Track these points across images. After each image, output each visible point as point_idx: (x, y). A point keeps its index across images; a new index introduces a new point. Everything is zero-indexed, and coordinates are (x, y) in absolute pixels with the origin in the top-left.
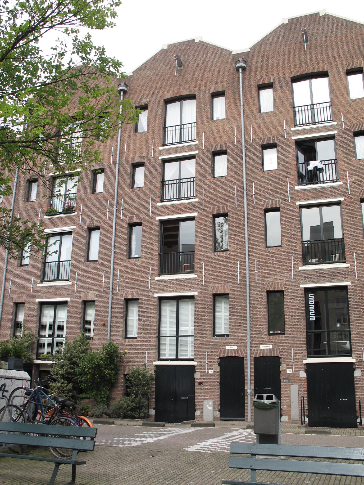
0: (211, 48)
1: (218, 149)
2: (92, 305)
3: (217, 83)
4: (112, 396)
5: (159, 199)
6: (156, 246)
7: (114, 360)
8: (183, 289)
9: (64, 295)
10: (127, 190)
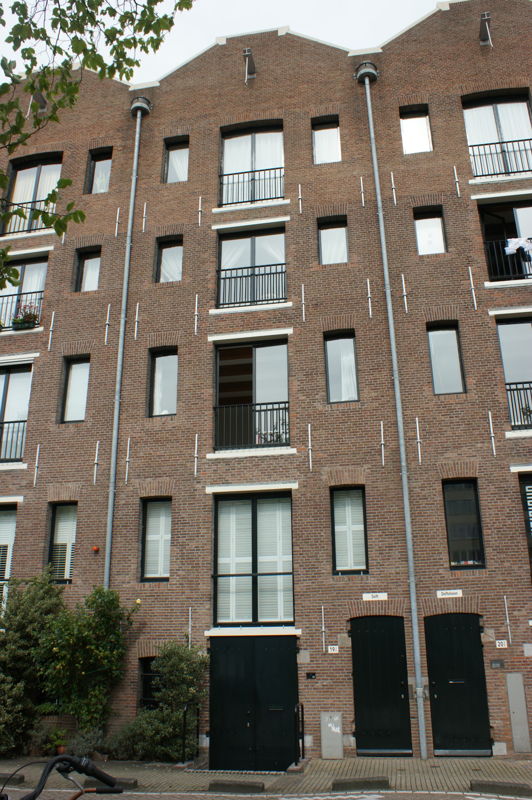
0: (309, 45)
1: (329, 213)
3: (321, 103)
5: (213, 302)
8: (269, 477)
9: (11, 490)
10: (148, 285)
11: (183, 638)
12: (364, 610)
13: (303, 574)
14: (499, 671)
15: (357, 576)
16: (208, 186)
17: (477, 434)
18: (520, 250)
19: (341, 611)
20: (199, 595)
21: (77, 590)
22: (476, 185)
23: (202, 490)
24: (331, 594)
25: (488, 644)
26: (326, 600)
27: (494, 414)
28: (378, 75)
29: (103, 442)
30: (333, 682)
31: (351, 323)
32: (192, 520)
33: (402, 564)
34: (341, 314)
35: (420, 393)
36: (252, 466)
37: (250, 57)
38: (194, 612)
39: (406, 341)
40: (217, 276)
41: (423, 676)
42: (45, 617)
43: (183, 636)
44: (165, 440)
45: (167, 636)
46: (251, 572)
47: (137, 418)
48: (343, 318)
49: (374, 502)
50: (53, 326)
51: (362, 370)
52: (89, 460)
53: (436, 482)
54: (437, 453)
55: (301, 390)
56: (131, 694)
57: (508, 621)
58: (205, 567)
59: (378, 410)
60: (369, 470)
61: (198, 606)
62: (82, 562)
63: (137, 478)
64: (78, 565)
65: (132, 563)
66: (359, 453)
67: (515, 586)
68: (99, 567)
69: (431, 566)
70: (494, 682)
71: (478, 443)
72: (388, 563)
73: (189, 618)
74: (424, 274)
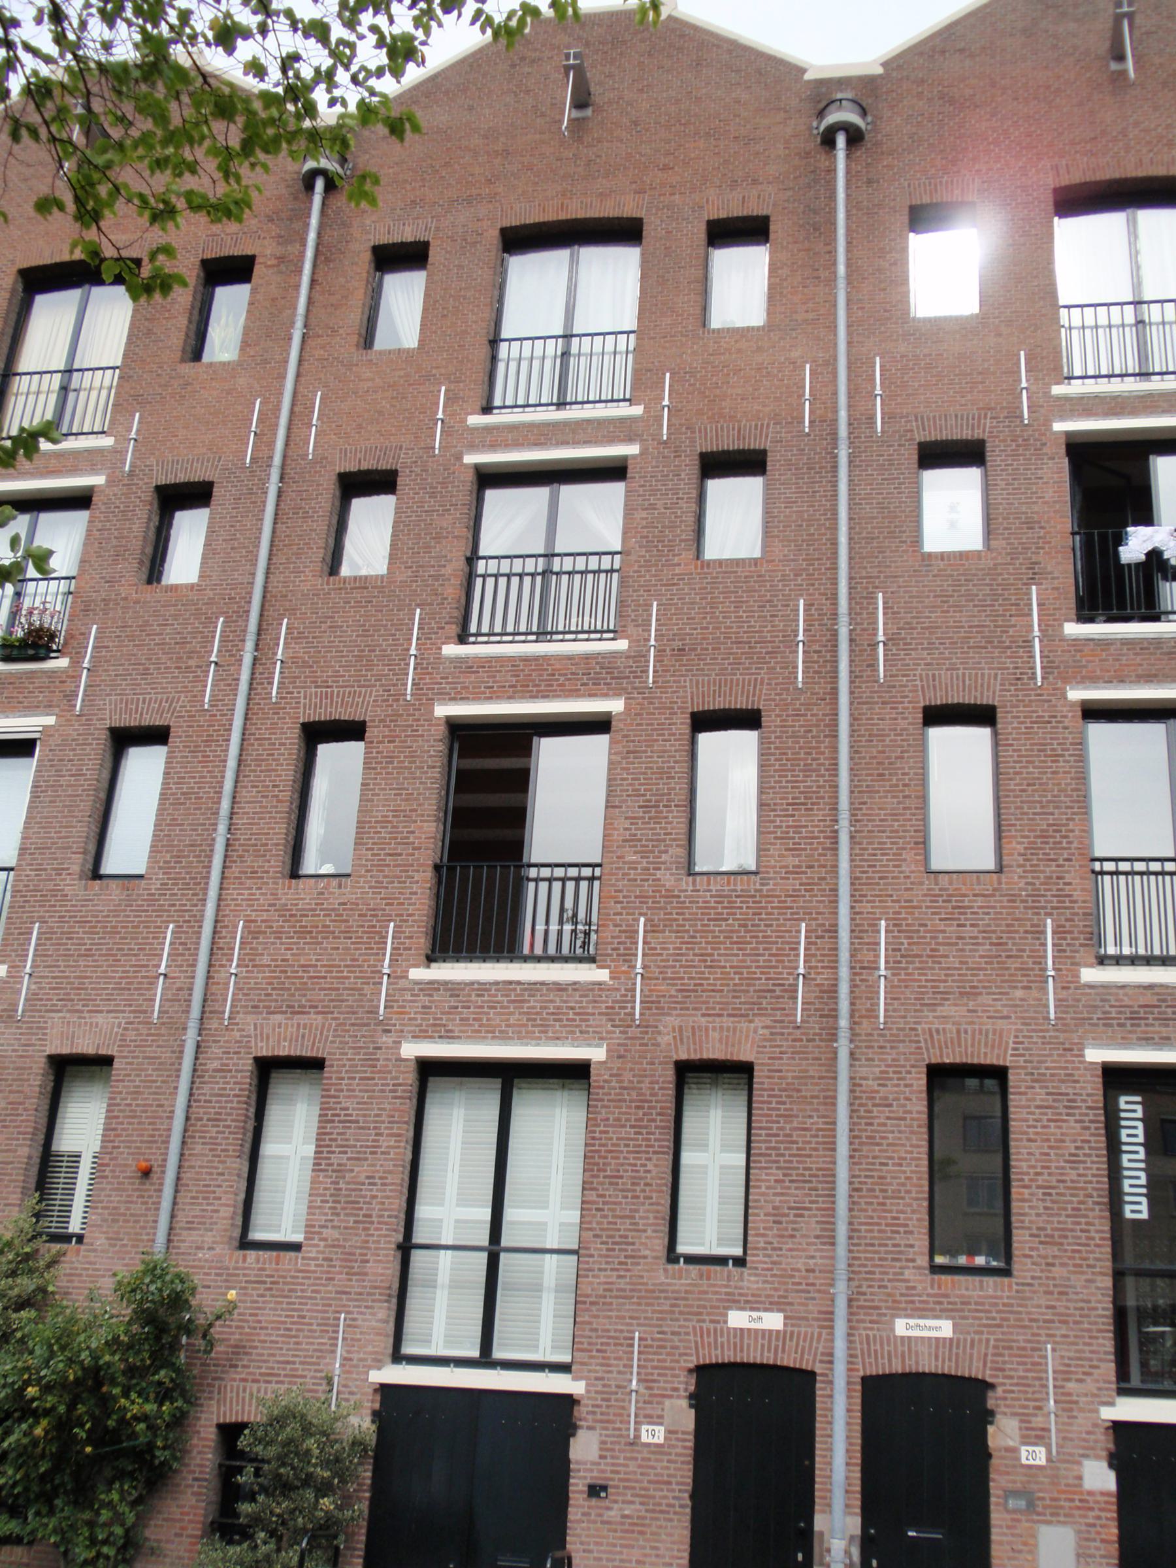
0: (718, 47)
1: (729, 442)
2: (91, 1078)
3: (734, 184)
4: (147, 1533)
5: (454, 630)
6: (425, 835)
7: (174, 1347)
10: (310, 576)
11: (321, 1385)
12: (729, 1349)
13: (600, 1256)
14: (1023, 1518)
15: (718, 1268)
16: (462, 362)
17: (1016, 969)
18: (1155, 555)
19: (677, 1348)
20: (365, 1287)
21: (93, 1259)
22: (1067, 399)
23: (392, 1048)
24: (659, 1304)
25: (1003, 1453)
26: (646, 1318)
27: (1059, 926)
28: (869, 127)
29: (181, 927)
30: (647, 1511)
31: (754, 695)
32: (365, 1116)
33: (822, 1250)
34: (735, 674)
35: (894, 866)
36: (509, 1002)
37: (579, 71)
38: (349, 1326)
39: (873, 746)
40: (467, 569)
41: (850, 1514)
42: (14, 1316)
43: (321, 1378)
44: (321, 932)
45: (285, 1376)
46: (486, 1243)
47: (262, 878)
48: (737, 685)
49: (770, 1103)
50: (92, 657)
51: (769, 805)
52: (147, 966)
53: (913, 1070)
54: (922, 1005)
55: (632, 840)
56: (192, 1507)
57: (1052, 1402)
58: (386, 1223)
59: (797, 896)
60: (766, 1031)
61: (361, 1313)
62: (110, 1196)
63: (250, 1013)
64: (101, 1202)
65: (221, 1205)
66: (748, 991)
67: (1076, 1322)
68: (148, 1209)
69: (886, 1259)
70: (1009, 1543)
71: (1016, 987)
72: (790, 1246)
73: (337, 1339)
74: (928, 597)
